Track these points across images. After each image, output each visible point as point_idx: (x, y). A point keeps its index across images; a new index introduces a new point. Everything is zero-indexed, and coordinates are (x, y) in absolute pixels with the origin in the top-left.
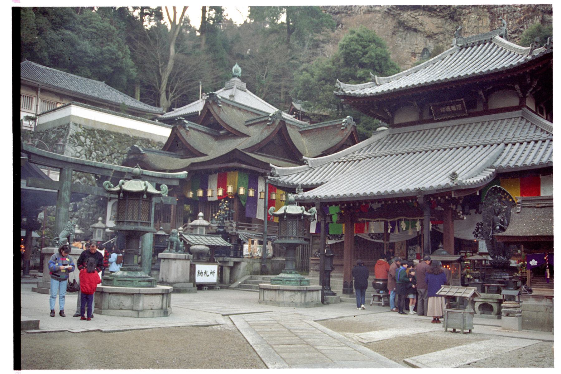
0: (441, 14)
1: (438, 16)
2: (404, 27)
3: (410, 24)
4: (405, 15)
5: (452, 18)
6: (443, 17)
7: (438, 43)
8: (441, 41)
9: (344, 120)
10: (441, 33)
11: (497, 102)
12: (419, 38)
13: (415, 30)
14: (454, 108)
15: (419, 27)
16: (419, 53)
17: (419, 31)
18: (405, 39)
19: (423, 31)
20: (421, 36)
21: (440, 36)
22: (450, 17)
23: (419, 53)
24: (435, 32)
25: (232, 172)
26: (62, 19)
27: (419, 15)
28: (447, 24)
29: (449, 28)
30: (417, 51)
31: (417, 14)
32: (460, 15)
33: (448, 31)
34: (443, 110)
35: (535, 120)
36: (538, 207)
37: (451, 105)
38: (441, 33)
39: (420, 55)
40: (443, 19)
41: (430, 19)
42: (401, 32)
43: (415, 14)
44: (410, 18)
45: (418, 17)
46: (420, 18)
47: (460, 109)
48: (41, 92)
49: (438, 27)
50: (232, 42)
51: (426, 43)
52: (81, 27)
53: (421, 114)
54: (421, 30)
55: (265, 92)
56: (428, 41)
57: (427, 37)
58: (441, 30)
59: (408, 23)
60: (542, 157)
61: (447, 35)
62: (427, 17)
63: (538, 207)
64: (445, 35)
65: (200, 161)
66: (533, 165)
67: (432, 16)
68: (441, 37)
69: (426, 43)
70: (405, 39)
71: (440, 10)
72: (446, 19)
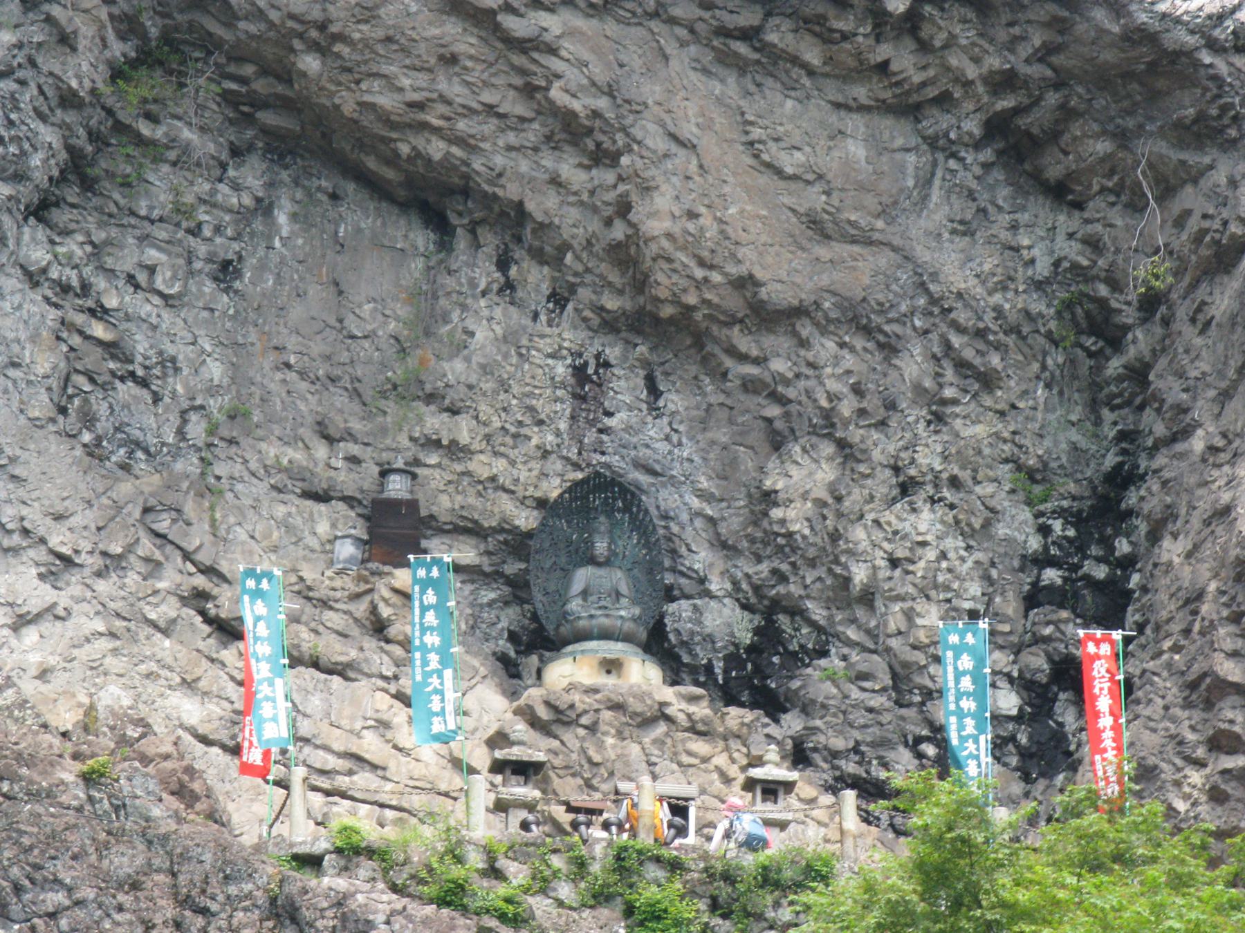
0: (904, 61)
2: (242, 108)
6: (908, 107)
7: (777, 442)
8: (827, 425)
10: (858, 320)
12: (487, 325)
13: (437, 202)
15: (517, 167)
18: (226, 271)
19: (573, 224)
21: (825, 347)
22: (996, 127)
23: (469, 529)
24: (776, 293)
26: (987, 524)
29: (960, 269)
30: (440, 493)
33: (939, 307)
36: (409, 812)
38: (858, 320)
39: (468, 553)
40: (898, 133)
49: (818, 227)
54: (542, 204)
55: (974, 185)
56: (624, 389)
58: (861, 273)
61: (913, 365)
62: (681, 61)
63: (409, 812)
64: (889, 349)
67: (775, 63)
70: (226, 271)
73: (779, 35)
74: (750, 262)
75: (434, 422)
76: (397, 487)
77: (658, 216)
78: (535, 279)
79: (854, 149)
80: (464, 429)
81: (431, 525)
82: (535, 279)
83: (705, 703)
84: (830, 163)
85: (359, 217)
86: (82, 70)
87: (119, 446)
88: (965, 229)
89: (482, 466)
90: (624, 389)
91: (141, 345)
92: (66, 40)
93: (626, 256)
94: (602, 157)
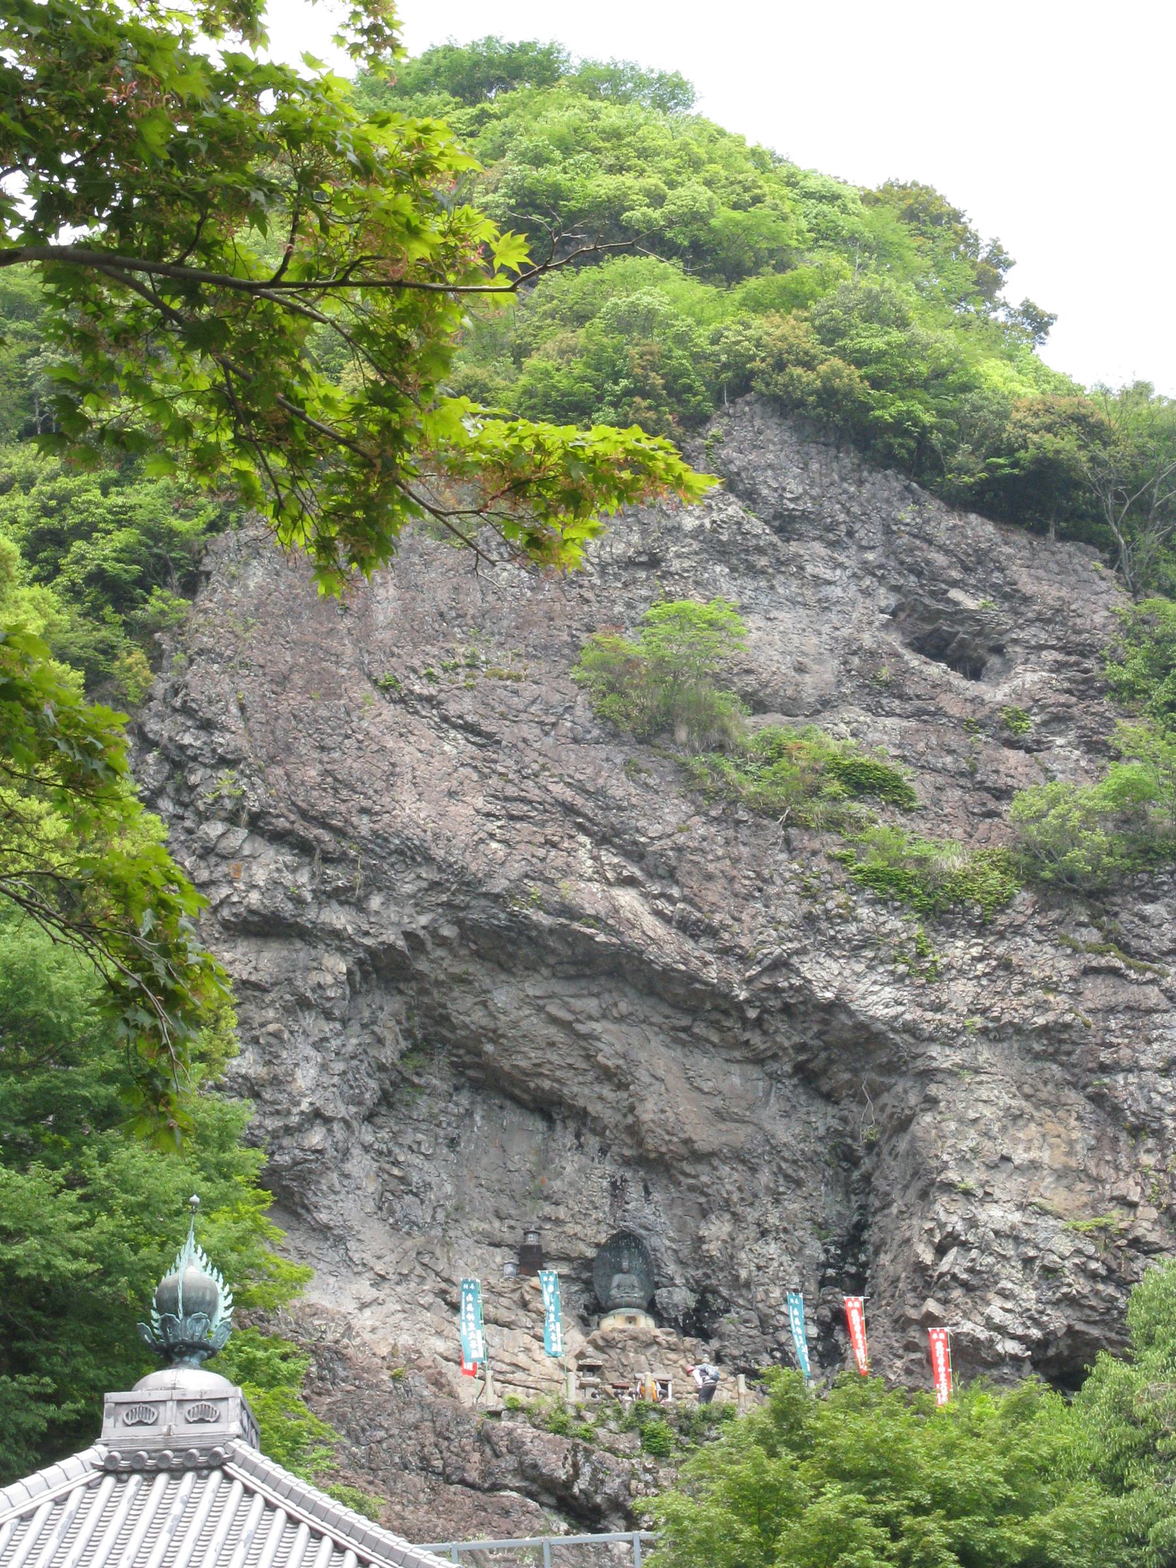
0: (756, 1039)
4: (502, 998)
6: (759, 1060)
7: (704, 1214)
8: (727, 1206)
10: (739, 1157)
12: (571, 1164)
13: (548, 1108)
17: (582, 1116)
18: (453, 1143)
19: (609, 1117)
21: (725, 1170)
22: (799, 1068)
24: (702, 1146)
28: (774, 1106)
29: (784, 1133)
30: (551, 1242)
31: (591, 1005)
32: (891, 1069)
33: (775, 1150)
38: (739, 1157)
40: (754, 1072)
41: (678, 1053)
42: (433, 1093)
43: (578, 1004)
45: (597, 1027)
49: (720, 1115)
50: (83, 1043)
52: (969, 885)
54: (595, 1108)
56: (634, 1192)
58: (739, 1136)
61: (765, 1177)
62: (656, 1042)
64: (754, 1170)
67: (699, 1042)
68: (730, 1178)
69: (617, 1190)
70: (453, 1143)
73: (700, 1029)
74: (689, 1132)
75: (548, 1209)
76: (532, 1240)
77: (648, 1112)
79: (735, 1079)
80: (562, 1212)
84: (724, 1086)
85: (512, 1117)
88: (786, 1115)
89: (570, 1228)
90: (634, 1192)
91: (415, 1178)
92: (380, 1041)
93: (633, 1130)
94: (622, 1086)
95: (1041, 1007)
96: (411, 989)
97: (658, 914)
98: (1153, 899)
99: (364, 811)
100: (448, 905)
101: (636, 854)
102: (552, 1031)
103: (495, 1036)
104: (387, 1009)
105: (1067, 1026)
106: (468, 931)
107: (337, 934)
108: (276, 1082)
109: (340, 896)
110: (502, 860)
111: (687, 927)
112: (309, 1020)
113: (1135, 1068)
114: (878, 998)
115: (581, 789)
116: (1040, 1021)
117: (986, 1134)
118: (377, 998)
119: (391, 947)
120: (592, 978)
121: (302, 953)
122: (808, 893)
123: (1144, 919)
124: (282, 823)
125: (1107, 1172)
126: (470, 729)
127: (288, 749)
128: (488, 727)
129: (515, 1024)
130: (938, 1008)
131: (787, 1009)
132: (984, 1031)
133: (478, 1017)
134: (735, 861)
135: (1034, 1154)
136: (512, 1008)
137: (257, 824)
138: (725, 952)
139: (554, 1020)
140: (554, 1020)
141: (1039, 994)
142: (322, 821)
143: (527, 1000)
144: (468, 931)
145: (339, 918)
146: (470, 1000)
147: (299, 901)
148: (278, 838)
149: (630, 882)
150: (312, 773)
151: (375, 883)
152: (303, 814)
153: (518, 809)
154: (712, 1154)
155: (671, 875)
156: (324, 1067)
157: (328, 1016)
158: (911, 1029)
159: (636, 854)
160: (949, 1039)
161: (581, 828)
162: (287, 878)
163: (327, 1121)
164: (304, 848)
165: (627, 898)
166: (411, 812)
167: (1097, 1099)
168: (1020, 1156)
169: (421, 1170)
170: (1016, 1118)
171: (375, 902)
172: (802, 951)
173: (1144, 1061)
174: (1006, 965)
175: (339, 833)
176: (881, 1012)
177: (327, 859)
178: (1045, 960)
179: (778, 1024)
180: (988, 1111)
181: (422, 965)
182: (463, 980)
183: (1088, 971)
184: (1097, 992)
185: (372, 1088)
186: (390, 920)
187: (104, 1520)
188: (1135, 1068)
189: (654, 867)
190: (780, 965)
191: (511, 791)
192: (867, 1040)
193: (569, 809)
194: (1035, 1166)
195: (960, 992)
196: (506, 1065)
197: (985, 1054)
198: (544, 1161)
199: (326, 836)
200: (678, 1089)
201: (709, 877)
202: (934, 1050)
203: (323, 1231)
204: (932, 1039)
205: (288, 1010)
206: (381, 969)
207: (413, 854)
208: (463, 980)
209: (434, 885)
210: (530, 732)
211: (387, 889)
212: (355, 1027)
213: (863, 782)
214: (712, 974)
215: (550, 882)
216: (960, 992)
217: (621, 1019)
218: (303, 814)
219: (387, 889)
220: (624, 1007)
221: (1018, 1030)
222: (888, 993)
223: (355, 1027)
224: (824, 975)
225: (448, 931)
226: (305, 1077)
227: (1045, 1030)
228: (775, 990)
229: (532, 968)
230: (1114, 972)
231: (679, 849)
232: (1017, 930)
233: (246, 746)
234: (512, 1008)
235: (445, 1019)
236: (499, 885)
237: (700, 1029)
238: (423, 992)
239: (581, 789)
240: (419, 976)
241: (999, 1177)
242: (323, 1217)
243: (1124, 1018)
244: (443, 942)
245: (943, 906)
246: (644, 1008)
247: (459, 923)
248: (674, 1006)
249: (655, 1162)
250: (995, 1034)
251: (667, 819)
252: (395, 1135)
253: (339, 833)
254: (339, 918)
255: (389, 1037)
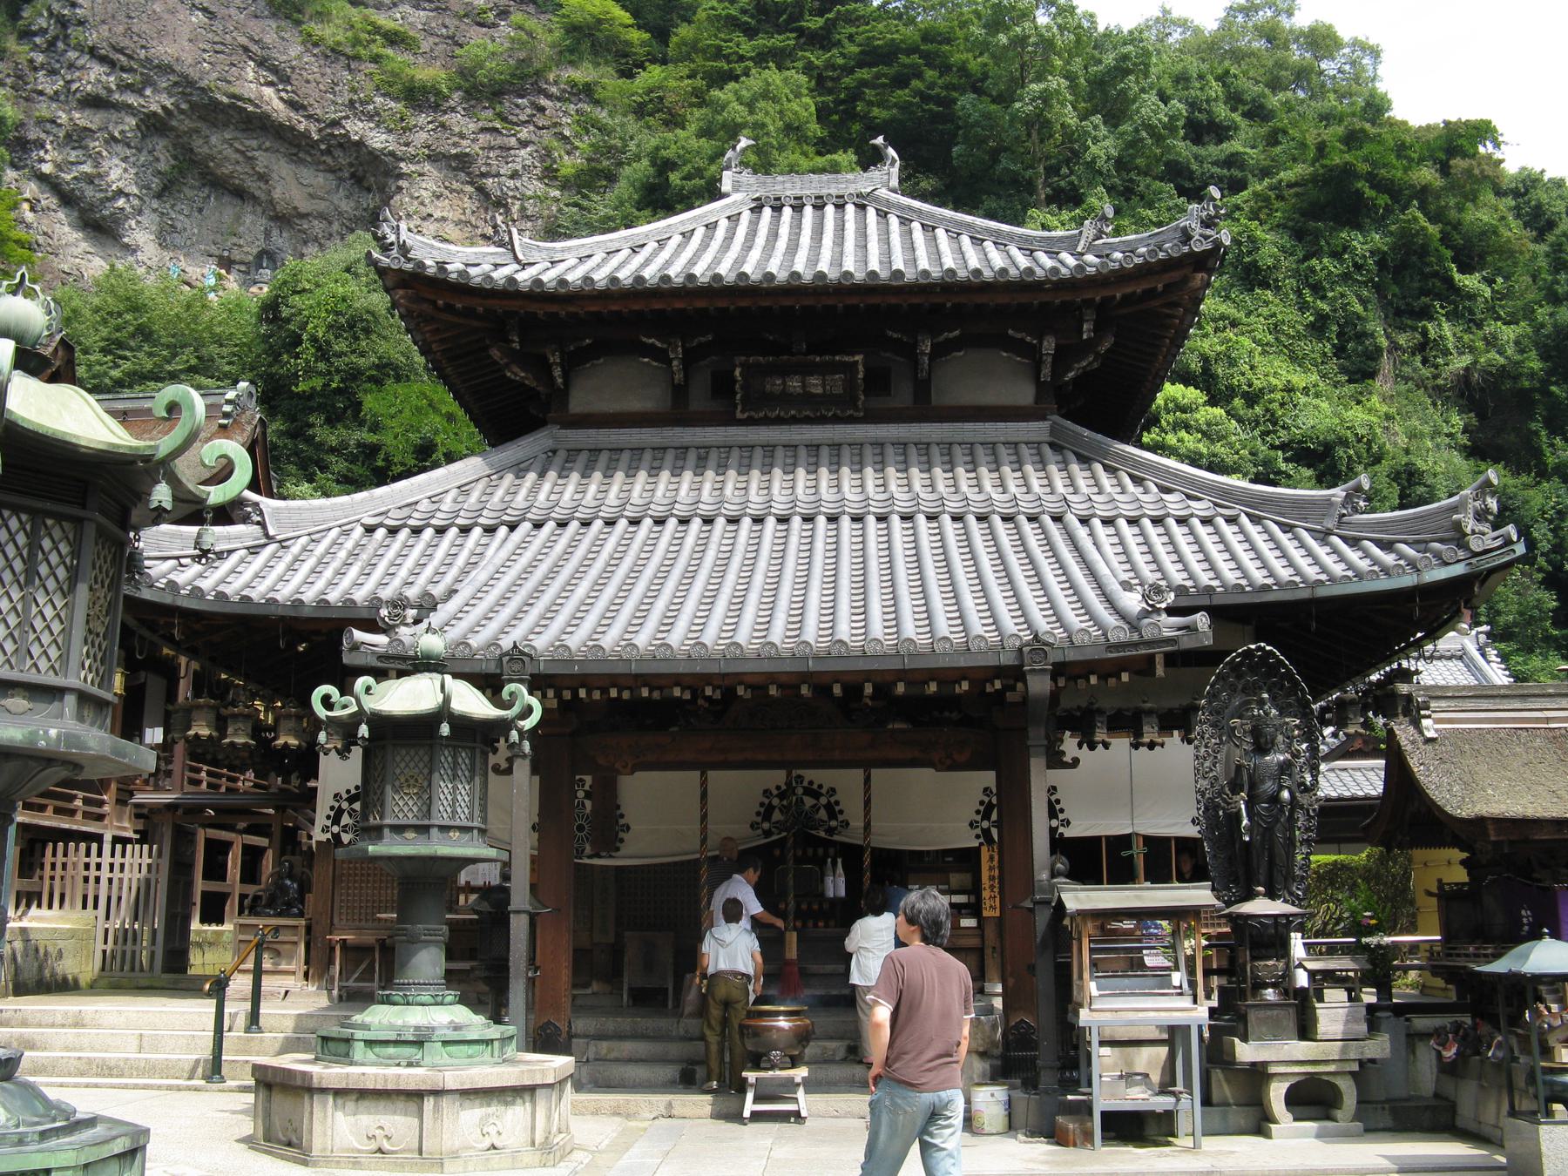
0: (329, 160)
1: (319, 163)
2: (203, 175)
3: (227, 169)
5: (358, 180)
6: (331, 171)
7: (305, 243)
8: (316, 240)
9: (231, 395)
10: (322, 216)
11: (967, 380)
12: (248, 219)
13: (240, 194)
14: (815, 384)
15: (252, 185)
16: (242, 263)
17: (255, 198)
18: (200, 210)
19: (263, 197)
20: (254, 213)
22: (353, 176)
23: (242, 263)
24: (302, 210)
25: (1021, 1137)
27: (260, 148)
29: (346, 206)
30: (236, 255)
31: (254, 143)
34: (775, 384)
35: (1126, 459)
37: (806, 370)
38: (322, 216)
39: (243, 268)
40: (330, 176)
42: (192, 187)
43: (248, 143)
44: (229, 152)
45: (256, 154)
46: (263, 160)
47: (839, 390)
48: (875, 1085)
49: (312, 196)
51: (267, 234)
53: (680, 392)
54: (257, 193)
56: (275, 232)
57: (271, 219)
58: (322, 206)
59: (219, 166)
60: (357, 585)
61: (336, 227)
62: (283, 162)
64: (330, 223)
65: (698, 430)
66: (246, 600)
67: (301, 162)
68: (317, 227)
69: (267, 234)
70: (200, 210)
71: (330, 146)
72: (341, 179)
73: (301, 155)
74: (296, 203)
75: (235, 240)
76: (226, 254)
77: (277, 194)
78: (259, 210)
79: (321, 180)
80: (242, 242)
81: (234, 262)
82: (259, 210)
83: (1202, 343)
84: (315, 183)
85: (226, 199)
86: (162, 166)
87: (1414, 354)
88: (347, 197)
89: (246, 249)
90: (275, 232)
91: (179, 225)
92: (158, 160)
93: (271, 202)
94: (267, 182)
95: (455, 145)
96: (172, 135)
97: (281, 99)
98: (522, 97)
99: (143, 47)
100: (183, 93)
101: (274, 70)
102: (238, 156)
103: (213, 159)
104: (160, 145)
105: (467, 155)
106: (193, 106)
107: (130, 106)
108: (100, 176)
109: (129, 87)
110: (208, 73)
111: (293, 105)
112: (119, 148)
113: (498, 175)
114: (378, 140)
115: (252, 39)
116: (454, 151)
117: (422, 204)
118: (155, 139)
119: (155, 114)
120: (253, 130)
121: (114, 116)
122: (353, 90)
123: (517, 106)
124: (103, 52)
125: (480, 223)
126: (205, 10)
127: (113, 17)
128: (212, 9)
129: (220, 152)
130: (407, 145)
131: (341, 145)
132: (429, 157)
133: (205, 150)
134: (323, 75)
135: (445, 214)
136: (218, 144)
137: (93, 52)
138: (309, 117)
139: (238, 151)
140: (238, 151)
141: (456, 139)
142: (121, 51)
143: (225, 141)
144: (193, 106)
145: (132, 99)
146: (201, 141)
147: (110, 91)
148: (103, 60)
149: (270, 84)
150: (121, 29)
151: (148, 81)
152: (114, 48)
153: (218, 47)
154: (307, 215)
155: (287, 80)
156: (125, 170)
157: (129, 146)
158: (392, 154)
159: (274, 70)
160: (412, 159)
161: (251, 58)
162: (104, 78)
163: (127, 195)
164: (112, 64)
165: (268, 92)
166: (165, 50)
167: (481, 190)
168: (438, 214)
169: (182, 222)
170: (438, 197)
171: (148, 92)
172: (347, 117)
173: (502, 171)
174: (443, 125)
175: (130, 57)
176: (378, 146)
177: (123, 69)
178: (457, 120)
179: (338, 153)
180: (424, 193)
181: (174, 123)
182: (197, 131)
183: (483, 130)
184: (484, 139)
185: (156, 184)
186: (156, 101)
187: (568, 553)
188: (498, 175)
189: (280, 76)
190: (336, 123)
191: (217, 39)
192: (374, 157)
193: (246, 49)
194: (444, 219)
195: (421, 137)
196: (219, 172)
197: (427, 167)
198: (238, 219)
199: (122, 58)
200: (292, 184)
201: (308, 82)
202: (402, 165)
203: (127, 247)
204: (402, 160)
205: (107, 142)
206: (153, 125)
207: (165, 69)
208: (197, 131)
209: (176, 84)
210: (233, 11)
211: (153, 84)
212: (145, 152)
213: (394, 39)
214: (302, 127)
215: (229, 82)
216: (421, 137)
217: (266, 150)
218: (114, 48)
219: (153, 84)
220: (268, 144)
221: (444, 156)
222: (384, 137)
223: (145, 152)
224: (356, 128)
225: (184, 106)
226: (114, 174)
227: (456, 156)
228: (332, 135)
229: (226, 125)
230: (495, 130)
231: (293, 68)
232: (453, 110)
233: (89, 13)
234: (218, 144)
235: (192, 150)
236: (203, 84)
237: (301, 155)
238: (178, 136)
239: (252, 39)
240: (173, 129)
241: (425, 224)
242: (126, 240)
243: (498, 152)
244: (182, 112)
245: (418, 97)
246: (276, 145)
247: (189, 102)
248: (290, 144)
249: (284, 219)
250: (434, 158)
251: (291, 51)
252: (173, 206)
253: (130, 57)
254: (132, 99)
255: (162, 158)
